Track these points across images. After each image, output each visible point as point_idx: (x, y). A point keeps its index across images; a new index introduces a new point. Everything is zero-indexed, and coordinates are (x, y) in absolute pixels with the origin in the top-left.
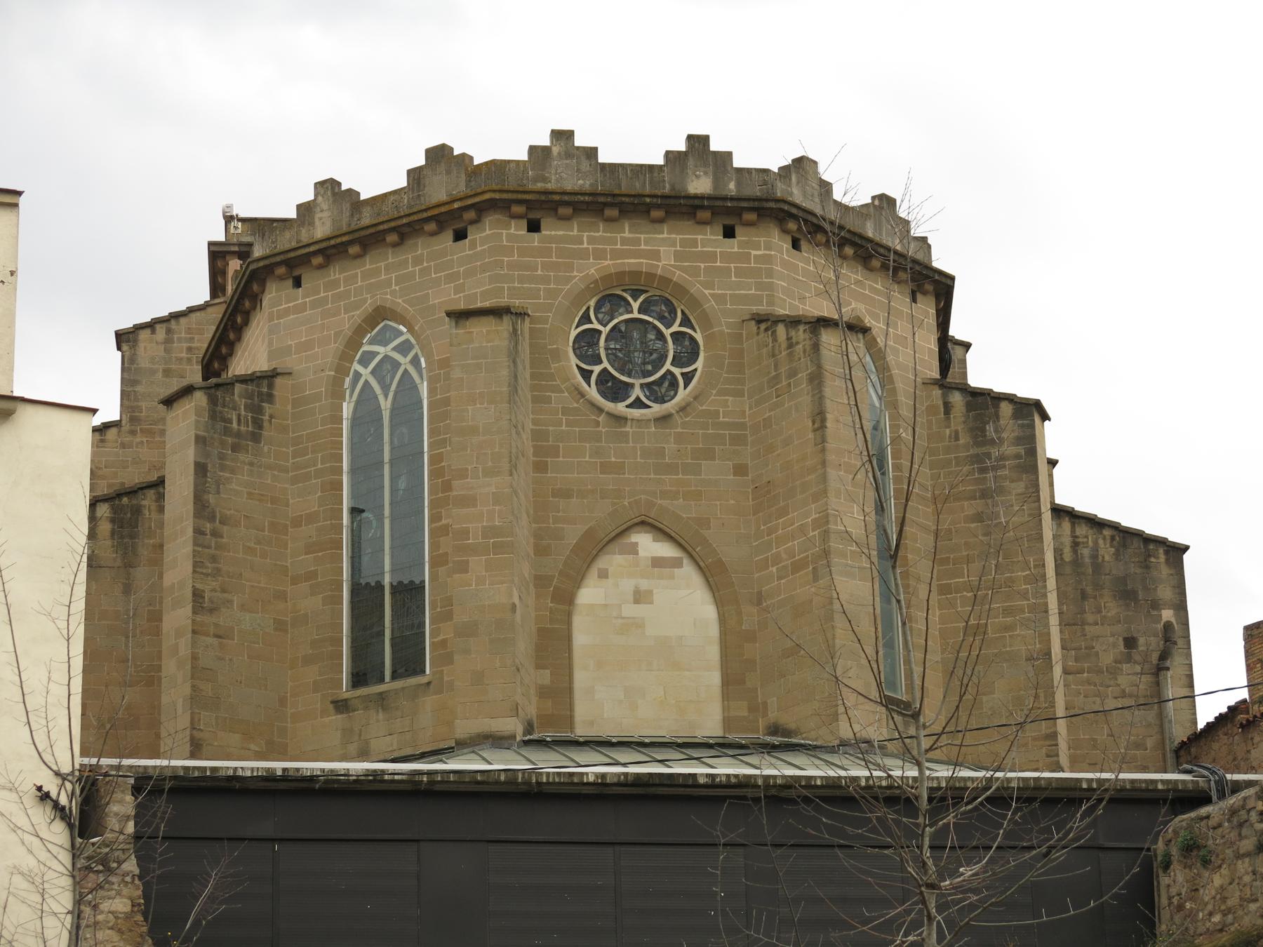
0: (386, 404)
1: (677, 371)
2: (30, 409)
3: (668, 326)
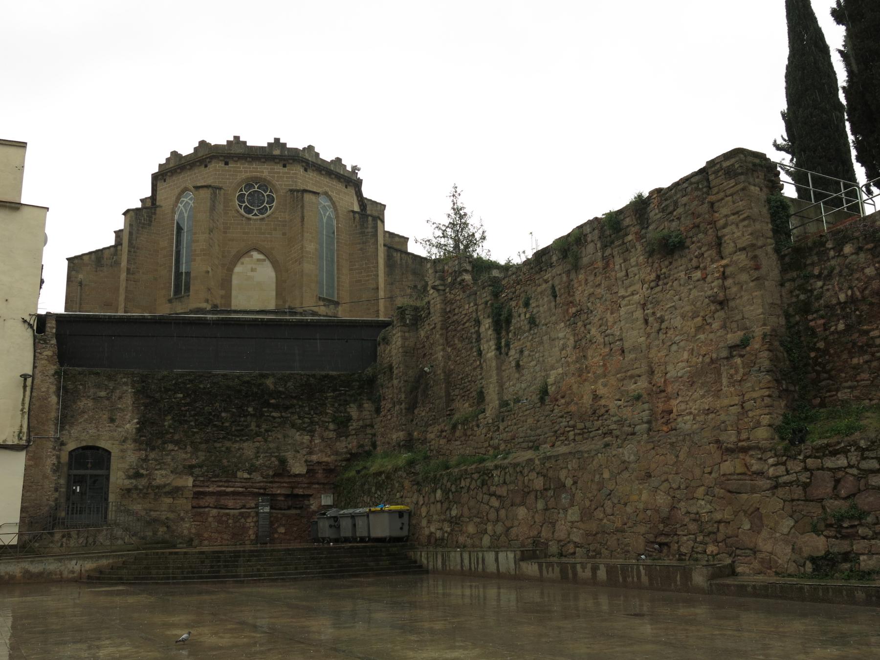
0: (186, 215)
1: (267, 206)
2: (26, 208)
3: (265, 193)
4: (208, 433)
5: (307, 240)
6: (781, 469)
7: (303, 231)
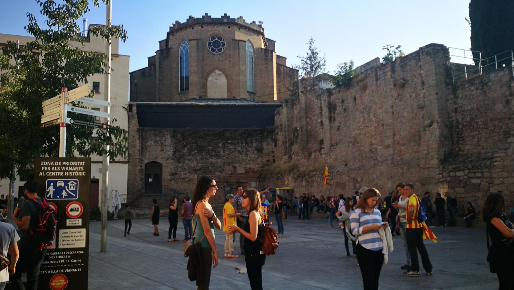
0: (184, 52)
1: (222, 47)
5: (241, 65)
6: (441, 176)
7: (239, 60)
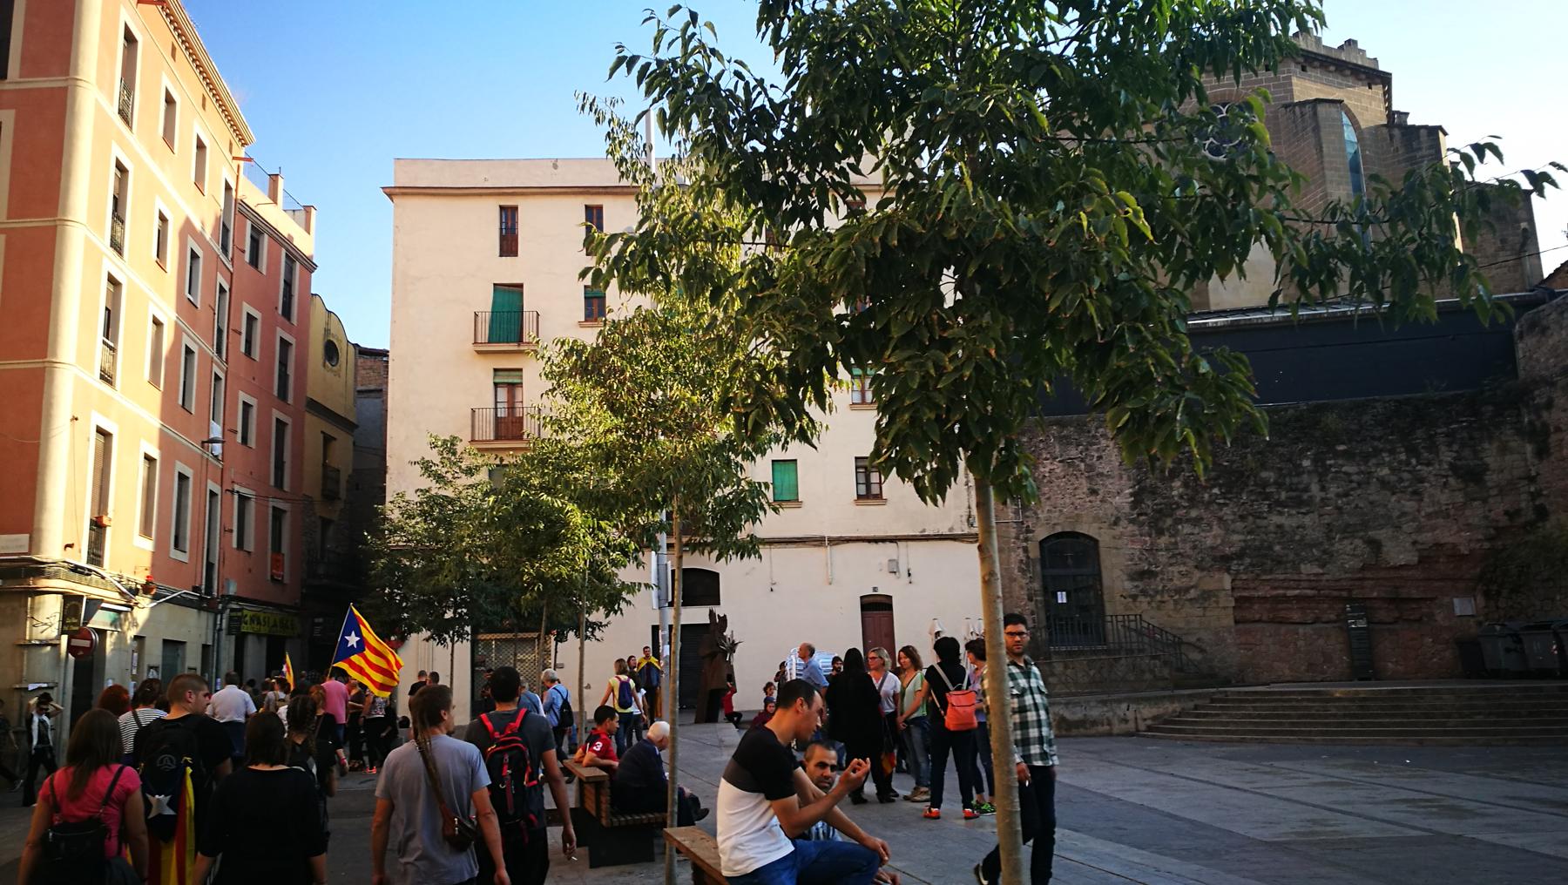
4: (1243, 503)
